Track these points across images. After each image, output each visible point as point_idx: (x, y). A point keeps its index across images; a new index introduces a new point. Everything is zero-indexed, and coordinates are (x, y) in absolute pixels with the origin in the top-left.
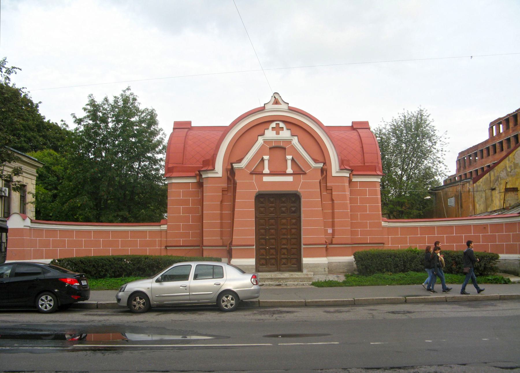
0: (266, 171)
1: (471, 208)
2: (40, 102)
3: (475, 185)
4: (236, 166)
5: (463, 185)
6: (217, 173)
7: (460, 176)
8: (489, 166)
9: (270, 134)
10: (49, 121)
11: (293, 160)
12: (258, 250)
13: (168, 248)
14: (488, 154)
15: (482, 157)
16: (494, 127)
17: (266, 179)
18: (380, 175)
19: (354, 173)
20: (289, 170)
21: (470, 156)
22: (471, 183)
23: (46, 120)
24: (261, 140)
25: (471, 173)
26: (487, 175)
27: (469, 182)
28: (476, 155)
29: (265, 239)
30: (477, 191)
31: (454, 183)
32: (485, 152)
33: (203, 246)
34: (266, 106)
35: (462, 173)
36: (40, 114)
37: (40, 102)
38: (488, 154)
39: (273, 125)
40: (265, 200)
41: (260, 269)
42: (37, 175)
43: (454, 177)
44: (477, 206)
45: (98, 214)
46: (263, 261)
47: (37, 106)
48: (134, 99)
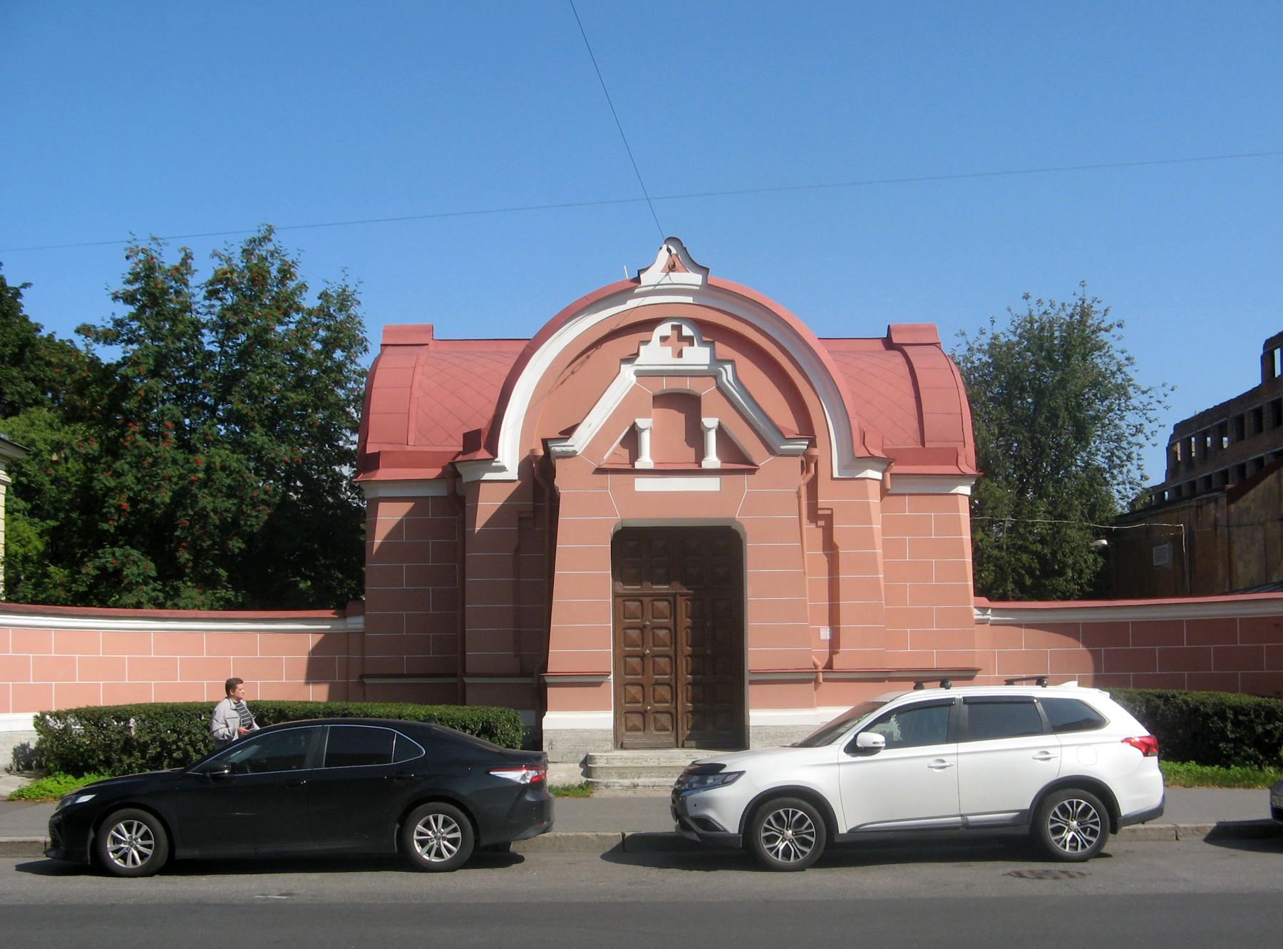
0: (645, 461)
1: (1221, 572)
2: (25, 286)
3: (1232, 507)
4: (558, 449)
5: (1199, 507)
6: (502, 469)
7: (1178, 489)
8: (1259, 462)
9: (655, 353)
10: (51, 336)
11: (721, 431)
12: (621, 686)
13: (367, 681)
14: (1259, 429)
15: (1241, 436)
16: (1277, 353)
17: (643, 485)
18: (971, 476)
19: (896, 469)
20: (712, 460)
21: (1205, 434)
22: (1223, 501)
23: (44, 333)
24: (627, 375)
25: (1208, 479)
26: (1270, 479)
27: (1216, 500)
28: (1222, 430)
29: (643, 657)
30: (1239, 526)
31: (1156, 507)
32: (1249, 423)
33: (465, 674)
34: (642, 276)
35: (1182, 481)
36: (25, 319)
37: (25, 286)
38: (1259, 429)
39: (665, 329)
40: (638, 550)
41: (626, 741)
42: (9, 480)
43: (1158, 490)
44: (1240, 568)
45: (873, 710)
46: (636, 720)
47: (17, 294)
48: (286, 273)
